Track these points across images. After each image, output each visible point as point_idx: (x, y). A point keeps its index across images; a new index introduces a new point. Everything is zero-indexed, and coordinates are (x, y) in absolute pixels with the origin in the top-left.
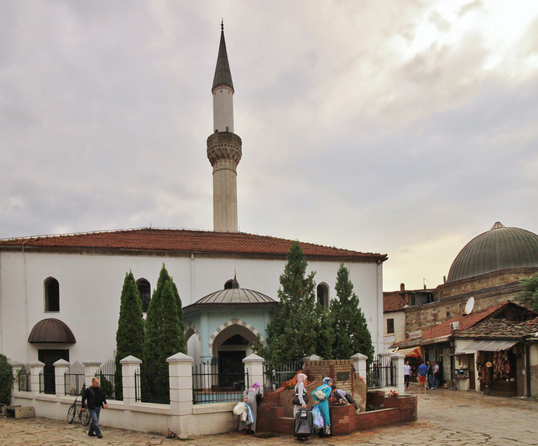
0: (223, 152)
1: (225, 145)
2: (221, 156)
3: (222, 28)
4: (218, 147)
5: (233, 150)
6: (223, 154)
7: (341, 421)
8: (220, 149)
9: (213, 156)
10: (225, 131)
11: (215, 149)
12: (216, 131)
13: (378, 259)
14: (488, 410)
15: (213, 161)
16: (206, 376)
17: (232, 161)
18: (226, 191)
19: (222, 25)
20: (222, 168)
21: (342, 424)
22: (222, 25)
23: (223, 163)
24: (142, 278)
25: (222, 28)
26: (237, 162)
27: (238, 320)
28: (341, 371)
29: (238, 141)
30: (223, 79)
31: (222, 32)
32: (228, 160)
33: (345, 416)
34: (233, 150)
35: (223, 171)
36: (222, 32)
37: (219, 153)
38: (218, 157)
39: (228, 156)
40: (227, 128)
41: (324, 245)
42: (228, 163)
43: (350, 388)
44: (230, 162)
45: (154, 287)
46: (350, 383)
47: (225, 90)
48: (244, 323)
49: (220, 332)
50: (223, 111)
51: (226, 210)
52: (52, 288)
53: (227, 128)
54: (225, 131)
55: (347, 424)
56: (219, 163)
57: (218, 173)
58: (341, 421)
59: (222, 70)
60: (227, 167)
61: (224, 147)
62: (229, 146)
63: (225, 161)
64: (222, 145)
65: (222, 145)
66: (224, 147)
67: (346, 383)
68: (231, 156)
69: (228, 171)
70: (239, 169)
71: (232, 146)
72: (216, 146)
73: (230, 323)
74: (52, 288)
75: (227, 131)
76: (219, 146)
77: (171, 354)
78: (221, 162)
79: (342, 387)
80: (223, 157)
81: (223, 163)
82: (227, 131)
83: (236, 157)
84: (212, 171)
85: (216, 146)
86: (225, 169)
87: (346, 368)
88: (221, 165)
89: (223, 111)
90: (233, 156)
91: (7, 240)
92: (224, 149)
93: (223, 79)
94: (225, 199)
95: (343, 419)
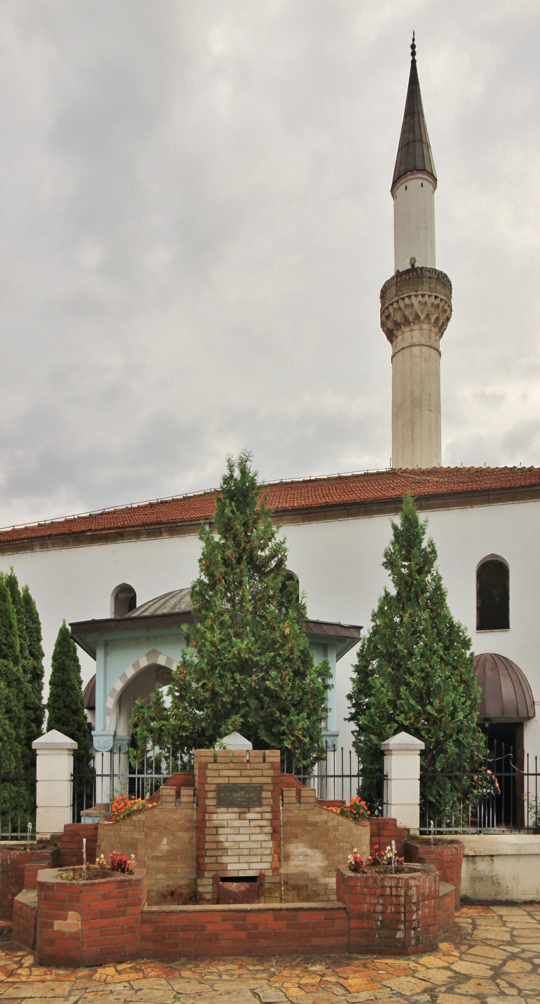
0: (407, 313)
1: (409, 297)
3: (413, 54)
4: (395, 305)
5: (426, 303)
6: (405, 317)
7: (58, 925)
8: (400, 308)
9: (390, 325)
10: (410, 267)
11: (391, 309)
12: (398, 271)
14: (62, 972)
15: (391, 335)
16: (331, 780)
17: (425, 326)
18: (412, 392)
19: (413, 47)
20: (405, 345)
21: (61, 933)
22: (413, 47)
24: (124, 583)
25: (413, 54)
26: (441, 328)
27: (158, 654)
28: (232, 781)
29: (442, 281)
30: (413, 159)
31: (414, 62)
32: (416, 327)
33: (71, 913)
34: (426, 303)
35: (407, 351)
36: (414, 62)
37: (398, 317)
38: (397, 325)
39: (417, 317)
40: (413, 261)
42: (416, 333)
43: (269, 830)
44: (421, 329)
46: (268, 816)
47: (414, 183)
48: (168, 659)
50: (413, 224)
51: (412, 431)
52: (493, 579)
53: (413, 261)
54: (410, 267)
55: (75, 936)
56: (400, 338)
58: (58, 925)
60: (415, 341)
61: (407, 301)
62: (416, 296)
63: (412, 330)
65: (403, 299)
66: (407, 301)
67: (250, 816)
68: (422, 317)
69: (416, 349)
71: (423, 296)
72: (392, 304)
73: (144, 663)
74: (493, 579)
75: (413, 266)
76: (397, 301)
78: (403, 333)
79: (236, 823)
80: (407, 322)
81: (408, 334)
82: (413, 266)
85: (392, 304)
87: (251, 773)
88: (403, 340)
89: (413, 224)
90: (428, 316)
92: (406, 305)
93: (413, 159)
94: (415, 405)
95: (65, 919)
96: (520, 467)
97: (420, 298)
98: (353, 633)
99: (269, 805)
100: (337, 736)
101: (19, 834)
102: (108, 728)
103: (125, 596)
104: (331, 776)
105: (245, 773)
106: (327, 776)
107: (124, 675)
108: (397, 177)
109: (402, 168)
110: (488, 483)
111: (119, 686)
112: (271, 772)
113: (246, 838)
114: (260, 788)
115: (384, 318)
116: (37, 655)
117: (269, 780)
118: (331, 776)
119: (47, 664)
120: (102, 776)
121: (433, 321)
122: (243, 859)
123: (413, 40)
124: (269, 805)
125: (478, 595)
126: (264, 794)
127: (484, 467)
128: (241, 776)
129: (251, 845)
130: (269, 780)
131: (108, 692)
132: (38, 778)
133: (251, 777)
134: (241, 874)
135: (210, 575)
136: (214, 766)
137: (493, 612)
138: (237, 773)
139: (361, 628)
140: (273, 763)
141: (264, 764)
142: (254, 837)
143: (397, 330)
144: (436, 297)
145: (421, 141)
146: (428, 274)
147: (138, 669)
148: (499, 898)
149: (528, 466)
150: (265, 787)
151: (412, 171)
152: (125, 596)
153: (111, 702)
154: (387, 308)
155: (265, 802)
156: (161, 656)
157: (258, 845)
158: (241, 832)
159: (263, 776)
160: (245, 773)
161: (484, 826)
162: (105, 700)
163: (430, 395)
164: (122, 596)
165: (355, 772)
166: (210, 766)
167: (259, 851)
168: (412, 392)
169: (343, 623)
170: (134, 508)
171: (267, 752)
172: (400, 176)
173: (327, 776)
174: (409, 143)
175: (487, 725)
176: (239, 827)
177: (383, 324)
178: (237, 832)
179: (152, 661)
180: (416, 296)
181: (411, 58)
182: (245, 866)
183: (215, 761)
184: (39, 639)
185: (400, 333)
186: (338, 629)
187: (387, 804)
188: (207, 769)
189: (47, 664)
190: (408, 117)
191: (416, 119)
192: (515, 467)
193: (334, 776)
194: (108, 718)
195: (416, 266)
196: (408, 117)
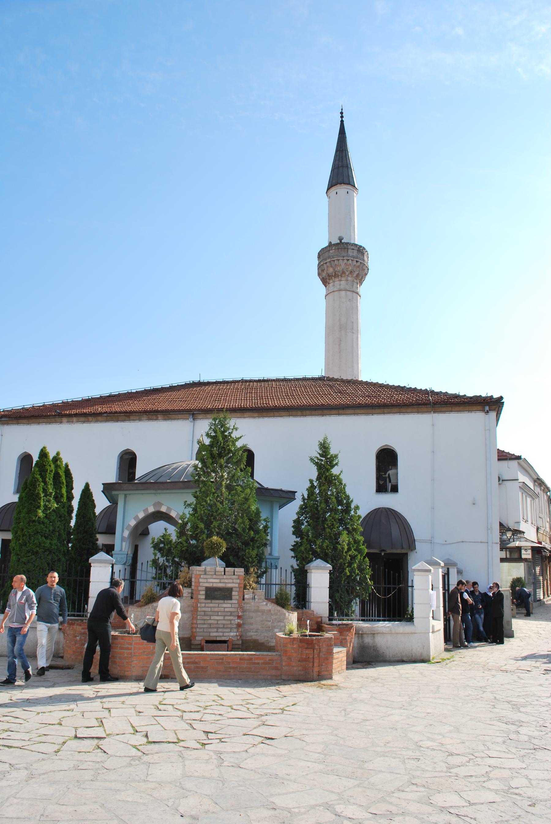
1: (338, 260)
2: (334, 274)
3: (342, 117)
4: (328, 264)
10: (339, 242)
12: (330, 243)
13: (492, 405)
15: (325, 282)
18: (340, 320)
19: (342, 113)
20: (335, 289)
22: (342, 113)
23: (337, 283)
25: (342, 117)
28: (215, 585)
31: (342, 122)
35: (336, 293)
36: (342, 122)
40: (341, 239)
41: (419, 388)
42: (343, 283)
45: (36, 458)
47: (342, 189)
48: (168, 508)
49: (138, 520)
50: (341, 216)
51: (340, 345)
52: (387, 459)
53: (341, 239)
56: (331, 285)
57: (331, 296)
59: (338, 168)
60: (342, 287)
63: (341, 280)
64: (334, 261)
69: (343, 293)
70: (363, 289)
74: (387, 459)
75: (341, 241)
77: (93, 555)
81: (337, 283)
83: (359, 272)
84: (325, 293)
86: (340, 290)
87: (226, 581)
88: (334, 285)
91: (81, 399)
93: (341, 174)
94: (342, 331)
96: (408, 387)
97: (345, 261)
98: (291, 495)
99: (236, 599)
100: (279, 559)
101: (76, 613)
102: (123, 550)
103: (128, 461)
104: (274, 584)
105: (223, 581)
106: (271, 584)
107: (137, 516)
108: (330, 186)
109: (334, 181)
110: (384, 398)
111: (133, 523)
112: (238, 581)
113: (222, 618)
114: (230, 590)
115: (320, 271)
116: (70, 497)
117: (237, 585)
118: (274, 584)
119: (75, 504)
120: (291, 585)
121: (355, 275)
122: (220, 630)
123: (342, 109)
124: (236, 599)
125: (377, 470)
126: (233, 593)
127: (385, 384)
128: (220, 582)
129: (224, 622)
130: (237, 585)
131: (125, 527)
132: (91, 580)
133: (226, 583)
134: (218, 639)
135: (203, 461)
136: (205, 576)
137: (385, 483)
138: (218, 581)
139: (296, 492)
140: (239, 576)
141: (234, 576)
142: (227, 618)
143: (329, 279)
144: (357, 261)
145: (347, 166)
146: (353, 247)
147: (147, 513)
148: (130, 561)
149: (413, 387)
150: (234, 589)
151: (341, 184)
152: (128, 461)
153: (126, 533)
154: (323, 265)
155: (233, 597)
156: (163, 506)
157: (229, 622)
158: (219, 614)
159: (233, 583)
160: (223, 581)
161: (372, 616)
162: (123, 531)
163: (353, 322)
164: (126, 457)
165: (293, 582)
166: (202, 576)
167: (229, 626)
168: (340, 320)
169: (284, 489)
170: (133, 393)
171: (236, 569)
172: (331, 185)
173: (271, 584)
174: (338, 168)
175: (383, 554)
176: (218, 612)
177: (319, 274)
178: (217, 614)
179: (157, 509)
180: (343, 260)
181: (341, 119)
182: (221, 634)
183: (205, 574)
184: (72, 489)
185: (331, 281)
186: (280, 493)
187: (309, 602)
188: (200, 578)
189: (75, 504)
190: (338, 152)
191: (344, 154)
192: (405, 387)
193: (276, 584)
194: (124, 544)
195: (343, 241)
196: (338, 152)
